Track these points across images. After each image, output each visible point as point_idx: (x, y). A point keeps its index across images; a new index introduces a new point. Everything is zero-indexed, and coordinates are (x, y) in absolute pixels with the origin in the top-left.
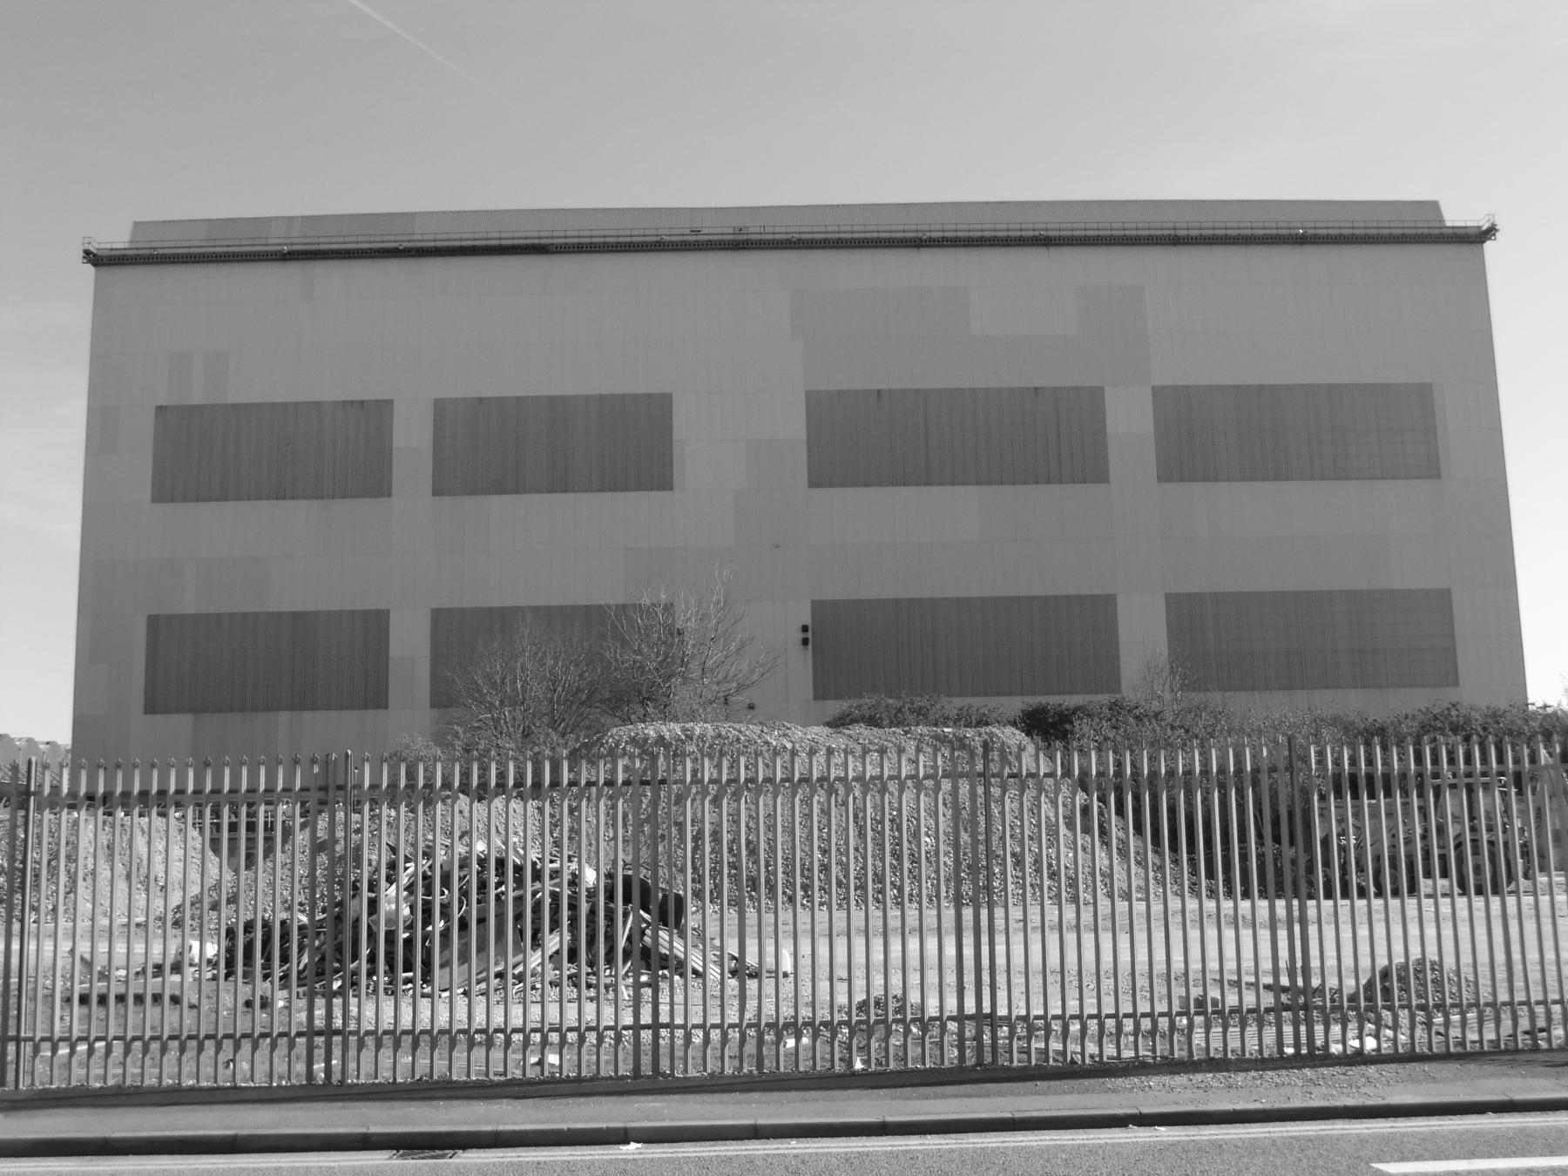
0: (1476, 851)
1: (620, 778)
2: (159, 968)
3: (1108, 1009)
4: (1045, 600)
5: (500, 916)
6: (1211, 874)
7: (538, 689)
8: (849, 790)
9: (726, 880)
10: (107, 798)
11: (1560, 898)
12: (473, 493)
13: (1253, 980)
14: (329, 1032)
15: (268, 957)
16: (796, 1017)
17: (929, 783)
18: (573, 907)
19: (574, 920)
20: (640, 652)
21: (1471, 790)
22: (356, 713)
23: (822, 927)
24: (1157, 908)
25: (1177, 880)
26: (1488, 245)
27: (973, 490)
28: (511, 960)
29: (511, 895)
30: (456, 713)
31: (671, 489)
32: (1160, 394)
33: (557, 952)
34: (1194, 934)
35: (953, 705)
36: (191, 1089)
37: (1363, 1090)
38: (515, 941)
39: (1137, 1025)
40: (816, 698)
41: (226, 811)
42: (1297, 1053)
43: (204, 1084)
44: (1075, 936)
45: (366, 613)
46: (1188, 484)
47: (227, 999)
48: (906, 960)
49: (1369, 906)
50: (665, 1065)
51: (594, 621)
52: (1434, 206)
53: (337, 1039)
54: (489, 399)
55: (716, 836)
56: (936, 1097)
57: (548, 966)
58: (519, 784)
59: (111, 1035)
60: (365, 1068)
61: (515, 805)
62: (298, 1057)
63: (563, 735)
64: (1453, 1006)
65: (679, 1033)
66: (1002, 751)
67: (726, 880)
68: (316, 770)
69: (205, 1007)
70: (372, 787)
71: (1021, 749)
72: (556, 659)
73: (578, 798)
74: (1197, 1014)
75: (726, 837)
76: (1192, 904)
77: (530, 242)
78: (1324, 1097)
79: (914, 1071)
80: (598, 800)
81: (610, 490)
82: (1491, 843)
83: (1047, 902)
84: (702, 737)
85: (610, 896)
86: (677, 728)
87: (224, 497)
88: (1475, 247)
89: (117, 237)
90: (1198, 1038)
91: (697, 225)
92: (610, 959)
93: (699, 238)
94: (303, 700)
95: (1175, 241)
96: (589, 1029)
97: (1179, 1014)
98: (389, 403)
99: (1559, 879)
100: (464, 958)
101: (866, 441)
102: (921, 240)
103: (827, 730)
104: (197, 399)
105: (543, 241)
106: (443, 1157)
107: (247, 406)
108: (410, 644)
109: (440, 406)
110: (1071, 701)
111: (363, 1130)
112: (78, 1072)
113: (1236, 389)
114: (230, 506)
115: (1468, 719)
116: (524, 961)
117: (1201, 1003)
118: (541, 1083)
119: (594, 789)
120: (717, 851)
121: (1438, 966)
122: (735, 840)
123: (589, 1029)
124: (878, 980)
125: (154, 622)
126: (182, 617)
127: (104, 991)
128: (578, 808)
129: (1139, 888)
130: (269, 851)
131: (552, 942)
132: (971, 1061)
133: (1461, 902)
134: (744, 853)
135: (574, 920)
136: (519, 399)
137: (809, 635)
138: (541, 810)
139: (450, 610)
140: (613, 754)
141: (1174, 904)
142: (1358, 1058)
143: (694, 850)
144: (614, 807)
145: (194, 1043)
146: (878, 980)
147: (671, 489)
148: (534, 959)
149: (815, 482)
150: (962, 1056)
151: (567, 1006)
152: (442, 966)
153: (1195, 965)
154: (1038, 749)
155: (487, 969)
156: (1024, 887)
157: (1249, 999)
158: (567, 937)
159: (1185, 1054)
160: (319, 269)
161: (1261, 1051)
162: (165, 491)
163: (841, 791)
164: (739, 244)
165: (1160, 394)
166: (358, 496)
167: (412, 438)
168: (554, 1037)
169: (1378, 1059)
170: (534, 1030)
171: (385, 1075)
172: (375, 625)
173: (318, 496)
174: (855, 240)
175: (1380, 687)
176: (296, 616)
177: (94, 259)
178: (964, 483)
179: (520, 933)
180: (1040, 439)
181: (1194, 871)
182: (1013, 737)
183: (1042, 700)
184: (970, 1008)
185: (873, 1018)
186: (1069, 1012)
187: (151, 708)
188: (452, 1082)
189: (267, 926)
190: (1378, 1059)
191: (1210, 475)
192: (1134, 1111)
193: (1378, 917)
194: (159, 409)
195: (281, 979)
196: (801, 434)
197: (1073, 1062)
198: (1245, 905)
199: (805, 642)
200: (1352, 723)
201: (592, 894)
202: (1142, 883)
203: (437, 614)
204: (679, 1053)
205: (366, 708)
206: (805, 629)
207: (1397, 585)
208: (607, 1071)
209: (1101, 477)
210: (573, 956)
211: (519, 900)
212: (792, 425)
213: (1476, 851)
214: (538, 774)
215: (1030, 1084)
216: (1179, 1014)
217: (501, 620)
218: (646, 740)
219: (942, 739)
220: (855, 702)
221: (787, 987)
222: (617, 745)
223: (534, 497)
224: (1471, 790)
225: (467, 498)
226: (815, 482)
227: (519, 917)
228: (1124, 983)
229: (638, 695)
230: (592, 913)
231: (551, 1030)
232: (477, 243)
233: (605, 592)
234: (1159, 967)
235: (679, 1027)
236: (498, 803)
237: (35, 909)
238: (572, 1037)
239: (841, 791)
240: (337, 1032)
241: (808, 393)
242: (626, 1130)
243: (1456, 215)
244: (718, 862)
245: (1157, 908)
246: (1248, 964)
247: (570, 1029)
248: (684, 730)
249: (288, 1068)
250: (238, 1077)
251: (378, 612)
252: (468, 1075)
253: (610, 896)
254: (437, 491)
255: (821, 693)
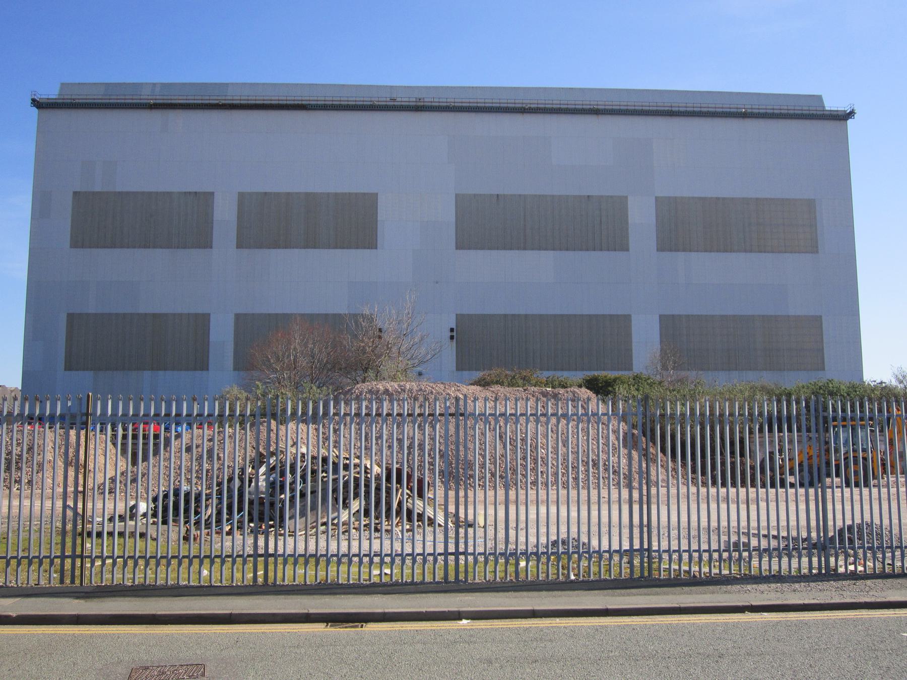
0: (856, 462)
1: (364, 412)
2: (122, 518)
3: (684, 547)
4: (590, 317)
5: (325, 490)
6: (704, 473)
7: (303, 362)
8: (497, 421)
9: (427, 471)
10: (41, 419)
11: (902, 489)
12: (261, 247)
13: (756, 532)
14: (267, 555)
15: (187, 510)
16: (516, 549)
17: (543, 419)
18: (367, 486)
19: (367, 493)
20: (363, 341)
21: (854, 429)
22: (190, 373)
23: (563, 499)
24: (673, 491)
25: (685, 475)
26: (850, 122)
27: (551, 253)
28: (331, 516)
29: (331, 477)
30: (256, 374)
31: (376, 248)
32: (660, 201)
33: (358, 511)
34: (703, 506)
35: (545, 375)
36: (186, 587)
37: (871, 593)
38: (333, 505)
39: (720, 556)
40: (458, 369)
41: (131, 427)
42: (820, 573)
43: (192, 584)
44: (736, 505)
45: (196, 315)
46: (674, 253)
47: (173, 536)
48: (601, 520)
49: (787, 492)
50: (462, 577)
51: (334, 322)
52: (819, 98)
53: (271, 560)
54: (271, 193)
55: (421, 446)
56: (628, 595)
57: (353, 519)
58: (305, 413)
59: (116, 555)
60: (289, 575)
61: (302, 426)
62: (238, 569)
63: (318, 387)
64: (887, 547)
65: (470, 558)
66: (896, 397)
67: (427, 471)
68: (259, 404)
69: (161, 540)
70: (177, 415)
71: (589, 399)
72: (314, 344)
73: (338, 423)
74: (744, 551)
75: (427, 447)
76: (693, 490)
77: (296, 102)
78: (851, 597)
79: (605, 580)
80: (351, 424)
81: (340, 248)
82: (865, 459)
83: (612, 487)
84: (411, 390)
85: (389, 479)
86: (396, 385)
87: (113, 246)
88: (842, 122)
89: (51, 92)
90: (755, 563)
91: (394, 96)
92: (388, 516)
93: (396, 103)
94: (158, 364)
95: (671, 113)
96: (397, 555)
97: (724, 551)
98: (212, 194)
99: (902, 480)
100: (303, 514)
101: (488, 224)
102: (525, 109)
103: (479, 388)
104: (98, 189)
105: (304, 103)
106: (357, 627)
107: (128, 193)
108: (222, 334)
109: (242, 196)
110: (611, 375)
111: (306, 611)
112: (107, 576)
113: (703, 199)
114: (117, 251)
115: (839, 389)
116: (338, 517)
117: (736, 545)
118: (392, 585)
119: (348, 418)
120: (422, 455)
121: (870, 525)
122: (432, 449)
123: (397, 555)
124: (563, 529)
125: (71, 317)
126: (88, 315)
127: (100, 529)
128: (339, 429)
129: (663, 480)
130: (156, 452)
131: (355, 505)
132: (637, 574)
133: (847, 491)
134: (437, 457)
135: (367, 493)
136: (288, 194)
137: (455, 334)
138: (317, 430)
139: (245, 315)
140: (358, 399)
141: (683, 490)
142: (854, 576)
143: (409, 454)
144: (360, 429)
145: (187, 560)
146: (563, 529)
147: (376, 248)
148: (344, 516)
149: (459, 247)
150: (255, 577)
151: (373, 541)
152: (290, 518)
153: (724, 523)
154: (598, 400)
155: (317, 521)
156: (598, 479)
157: (764, 544)
158: (363, 503)
159: (142, 580)
160: (172, 114)
161: (790, 571)
162: (78, 242)
163: (493, 423)
164: (418, 108)
165: (660, 201)
166: (192, 248)
167: (225, 213)
168: (377, 560)
169: (865, 577)
170: (365, 555)
171: (299, 580)
172: (201, 322)
173: (169, 246)
174: (486, 108)
175: (780, 370)
176: (155, 316)
177: (37, 104)
178: (546, 249)
179: (336, 500)
180: (592, 226)
181: (694, 471)
182: (585, 393)
183: (596, 373)
184: (626, 546)
185: (562, 551)
186: (682, 548)
187: (69, 367)
188: (339, 584)
189: (177, 493)
190: (865, 577)
191: (687, 248)
192: (747, 604)
193: (802, 499)
194: (75, 193)
195: (195, 524)
196: (453, 219)
197: (695, 576)
198: (723, 491)
199: (452, 338)
200: (772, 390)
201: (378, 478)
202: (665, 478)
203: (238, 317)
204: (470, 570)
205: (195, 369)
206: (452, 330)
207: (792, 312)
208: (428, 578)
209: (625, 248)
210: (367, 513)
211: (335, 481)
212: (449, 215)
213: (856, 462)
214: (315, 409)
215: (678, 589)
216: (724, 551)
217: (278, 323)
218: (378, 391)
219: (545, 395)
220: (486, 372)
221: (480, 532)
222: (361, 394)
223: (296, 251)
224: (854, 429)
225: (256, 250)
226: (459, 247)
227: (335, 490)
228: (684, 533)
229: (364, 366)
230: (378, 489)
231: (375, 555)
232: (265, 102)
233: (341, 308)
234: (704, 523)
235: (471, 554)
236: (292, 425)
237: (19, 482)
238: (387, 559)
239: (493, 423)
240: (271, 555)
241: (457, 195)
242: (459, 612)
243: (831, 104)
244: (422, 461)
245: (673, 491)
246: (764, 523)
247: (386, 555)
248: (400, 386)
249: (244, 575)
250: (213, 580)
251: (203, 315)
252: (349, 581)
253: (389, 479)
254: (239, 246)
255: (460, 367)
